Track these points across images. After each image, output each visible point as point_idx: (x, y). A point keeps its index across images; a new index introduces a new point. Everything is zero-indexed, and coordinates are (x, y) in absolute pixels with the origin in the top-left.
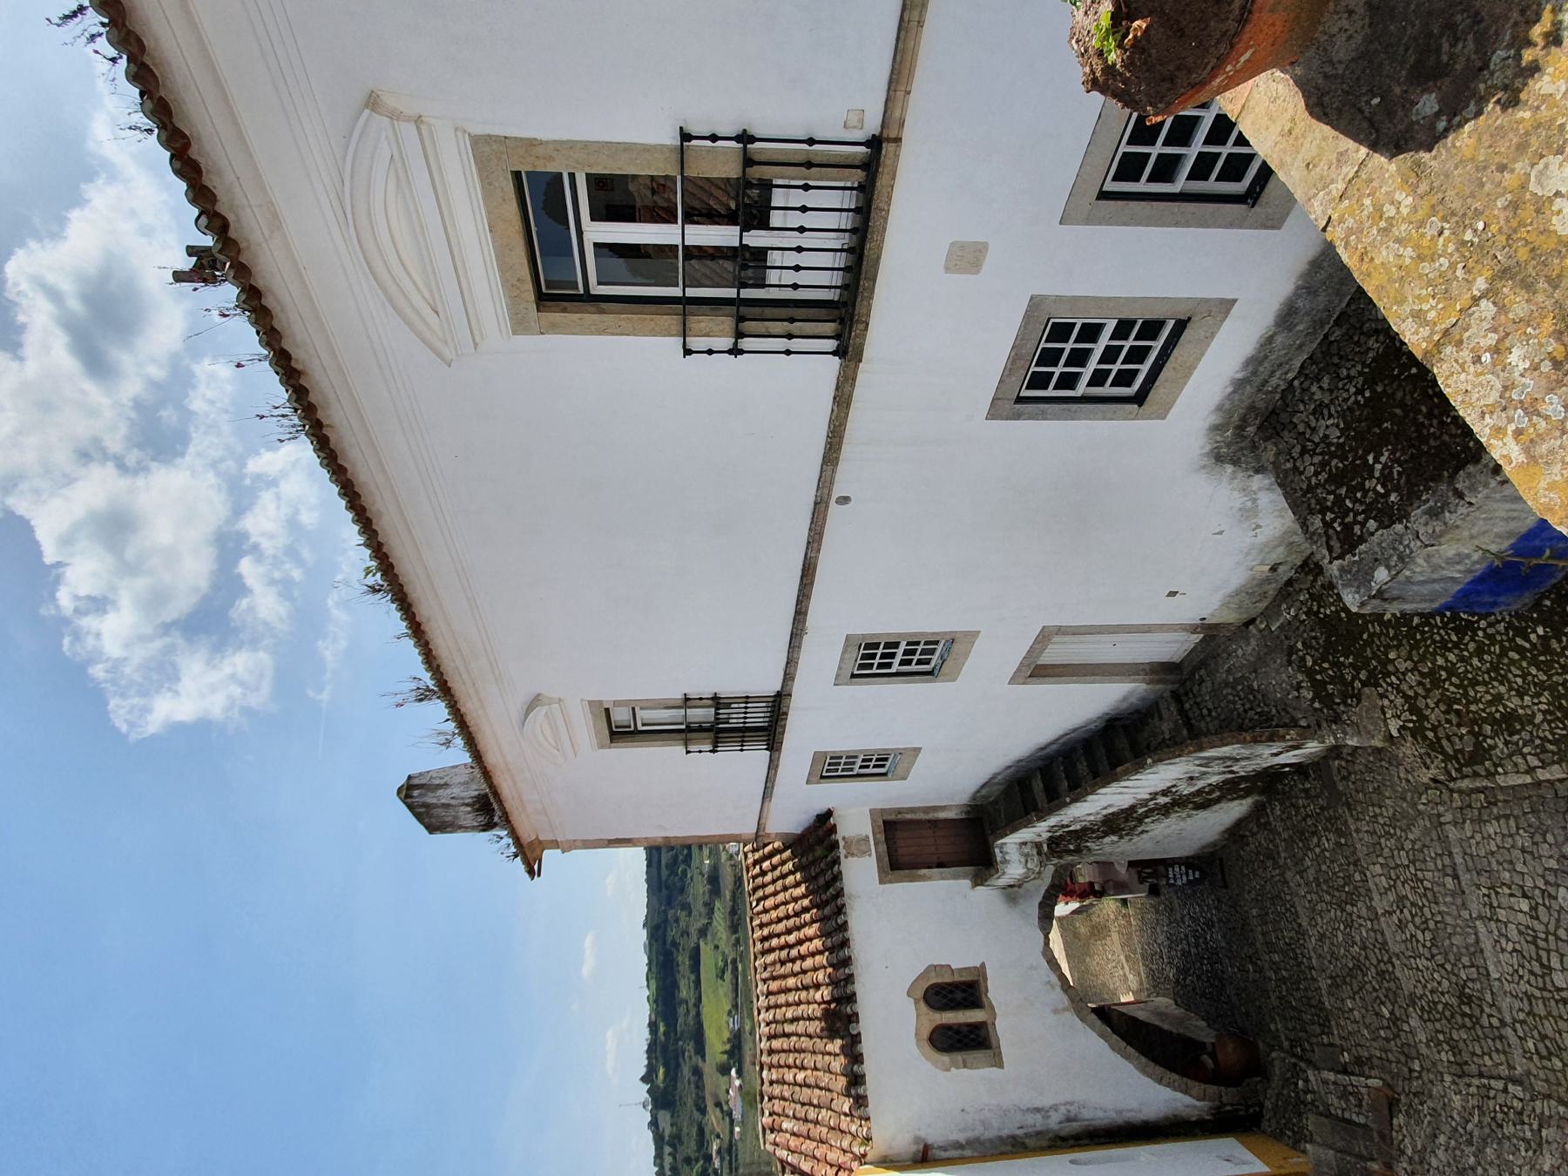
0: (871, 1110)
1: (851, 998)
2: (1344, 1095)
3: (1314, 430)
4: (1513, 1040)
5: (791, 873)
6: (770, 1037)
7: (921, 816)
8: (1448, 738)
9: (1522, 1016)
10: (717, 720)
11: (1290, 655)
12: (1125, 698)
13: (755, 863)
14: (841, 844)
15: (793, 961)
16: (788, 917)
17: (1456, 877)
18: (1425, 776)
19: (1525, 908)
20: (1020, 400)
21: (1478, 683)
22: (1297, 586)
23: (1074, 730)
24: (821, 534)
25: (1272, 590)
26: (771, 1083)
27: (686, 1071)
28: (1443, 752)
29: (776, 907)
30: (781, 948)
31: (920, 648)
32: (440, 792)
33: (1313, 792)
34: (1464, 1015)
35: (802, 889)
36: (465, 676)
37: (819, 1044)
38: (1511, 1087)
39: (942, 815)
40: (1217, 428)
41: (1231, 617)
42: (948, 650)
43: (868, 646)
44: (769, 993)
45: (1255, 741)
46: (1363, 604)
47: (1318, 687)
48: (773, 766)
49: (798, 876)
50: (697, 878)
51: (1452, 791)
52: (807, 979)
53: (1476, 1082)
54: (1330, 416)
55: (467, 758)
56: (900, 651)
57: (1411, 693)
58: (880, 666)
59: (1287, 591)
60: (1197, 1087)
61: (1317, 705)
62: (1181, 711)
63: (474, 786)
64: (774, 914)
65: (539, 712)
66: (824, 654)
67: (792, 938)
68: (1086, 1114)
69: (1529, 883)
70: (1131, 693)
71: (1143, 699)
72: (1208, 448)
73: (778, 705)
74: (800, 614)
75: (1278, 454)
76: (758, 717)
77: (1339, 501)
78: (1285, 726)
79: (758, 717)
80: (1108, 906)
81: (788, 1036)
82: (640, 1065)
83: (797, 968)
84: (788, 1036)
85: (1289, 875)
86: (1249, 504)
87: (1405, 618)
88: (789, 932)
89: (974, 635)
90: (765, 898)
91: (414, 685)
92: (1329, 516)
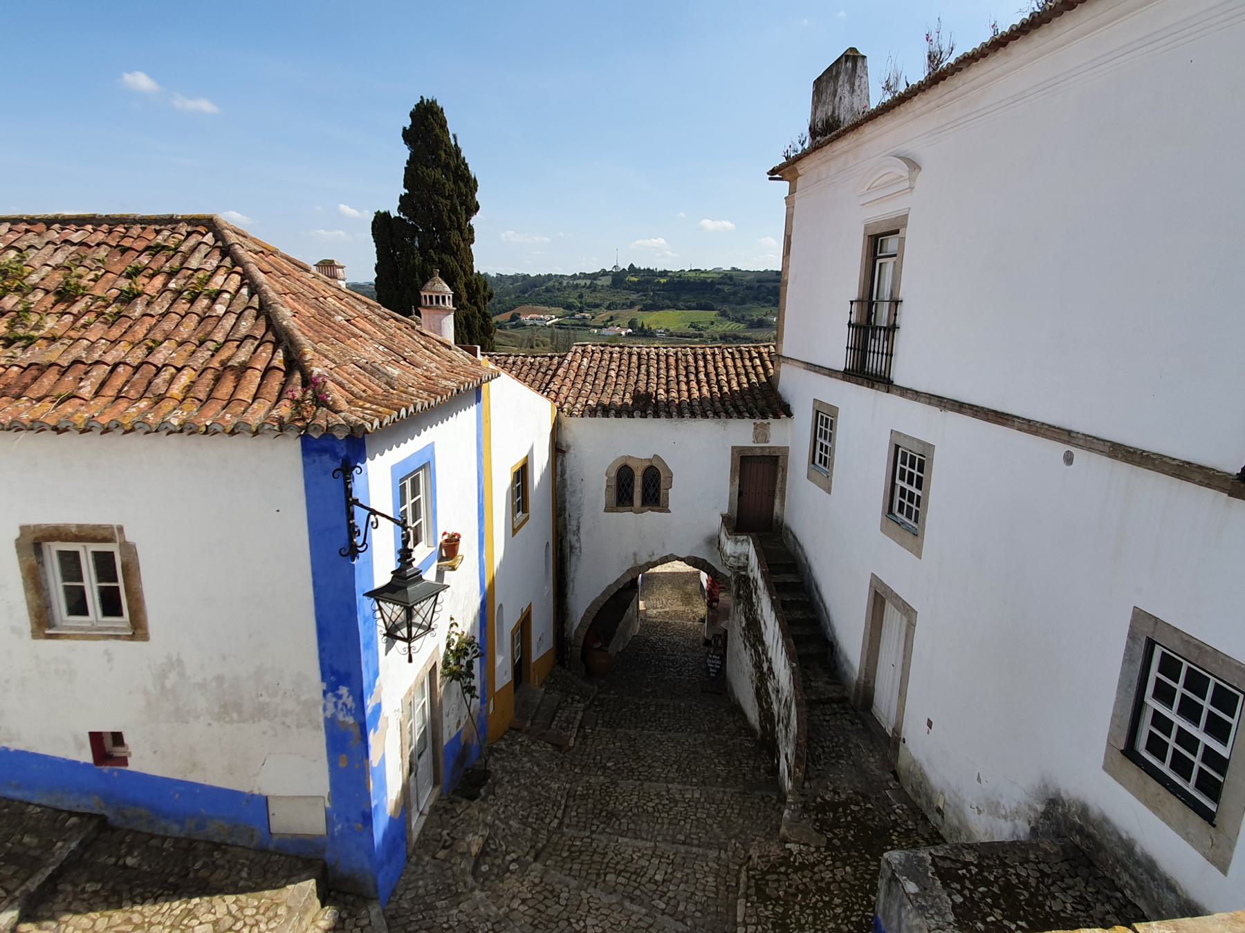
0: (587, 419)
1: (656, 415)
2: (568, 722)
3: (1064, 890)
4: (583, 834)
5: (749, 380)
6: (639, 354)
7: (779, 486)
8: (778, 881)
9: (594, 845)
10: (875, 328)
11: (862, 796)
12: (847, 661)
13: (760, 354)
14: (765, 421)
15: (687, 376)
16: (717, 375)
17: (684, 843)
18: (754, 853)
19: (658, 877)
20: (1151, 644)
21: (815, 920)
22: (921, 822)
23: (828, 616)
24: (1036, 433)
25: (921, 802)
26: (611, 353)
27: (634, 297)
28: (768, 872)
29: (725, 366)
30: (696, 368)
31: (914, 506)
32: (847, 87)
33: (757, 773)
34: (601, 811)
35: (735, 387)
36: (947, 97)
37: (631, 389)
38: (556, 821)
39: (777, 502)
40: (1084, 811)
41: (903, 762)
42: (908, 530)
43: (921, 463)
44: (667, 356)
45: (798, 746)
46: (889, 863)
47: (833, 806)
48: (831, 373)
49: (746, 386)
50: (764, 311)
51: (741, 866)
52: (673, 385)
53: (563, 802)
54: (1075, 910)
55: (873, 106)
56: (913, 489)
57: (816, 869)
58: (903, 470)
59: (918, 814)
60: (583, 633)
61: (819, 800)
62: (830, 701)
63: (848, 118)
64: (720, 364)
65: (902, 170)
66: (919, 423)
67: (702, 376)
68: (574, 559)
69: (671, 887)
70: (851, 666)
71: (845, 674)
72: (1064, 795)
73: (882, 381)
74: (960, 407)
75: (1045, 851)
76: (874, 363)
77: (987, 883)
78: (807, 772)
79: (874, 363)
80: (702, 610)
81: (639, 368)
82: (641, 265)
83: (682, 378)
84: (639, 368)
85: (704, 736)
86: (1003, 812)
87: (874, 890)
88: (707, 375)
89: (919, 555)
90: (733, 359)
91: (945, 48)
92: (974, 870)
